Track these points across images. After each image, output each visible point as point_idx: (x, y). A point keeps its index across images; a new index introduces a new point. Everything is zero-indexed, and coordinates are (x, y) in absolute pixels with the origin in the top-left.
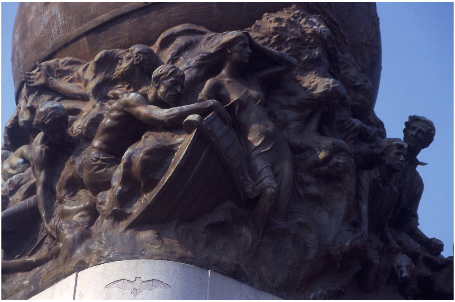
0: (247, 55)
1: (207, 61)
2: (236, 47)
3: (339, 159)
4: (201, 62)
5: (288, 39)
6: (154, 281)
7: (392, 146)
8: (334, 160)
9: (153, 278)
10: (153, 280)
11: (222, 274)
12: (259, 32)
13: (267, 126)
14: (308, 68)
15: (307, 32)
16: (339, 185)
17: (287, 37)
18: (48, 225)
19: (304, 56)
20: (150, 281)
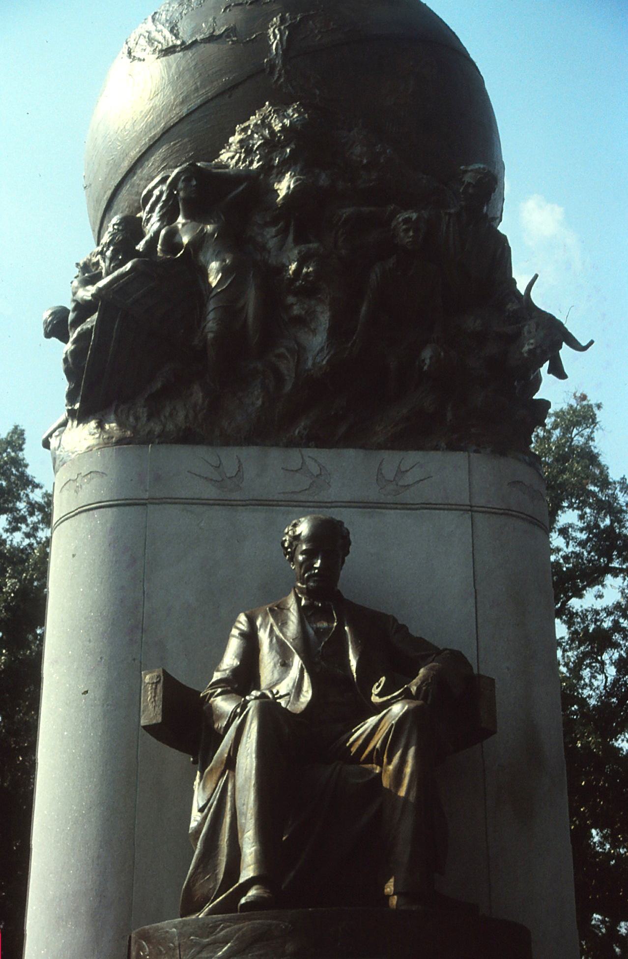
0: (194, 188)
1: (164, 210)
2: (181, 185)
3: (309, 268)
4: (161, 213)
5: (256, 146)
6: (92, 474)
7: (399, 224)
8: (304, 271)
9: (91, 470)
10: (91, 472)
11: (171, 443)
12: (231, 152)
13: (224, 260)
14: (283, 171)
15: (276, 131)
16: (319, 296)
17: (253, 145)
18: (561, 556)
19: (276, 160)
20: (88, 474)
